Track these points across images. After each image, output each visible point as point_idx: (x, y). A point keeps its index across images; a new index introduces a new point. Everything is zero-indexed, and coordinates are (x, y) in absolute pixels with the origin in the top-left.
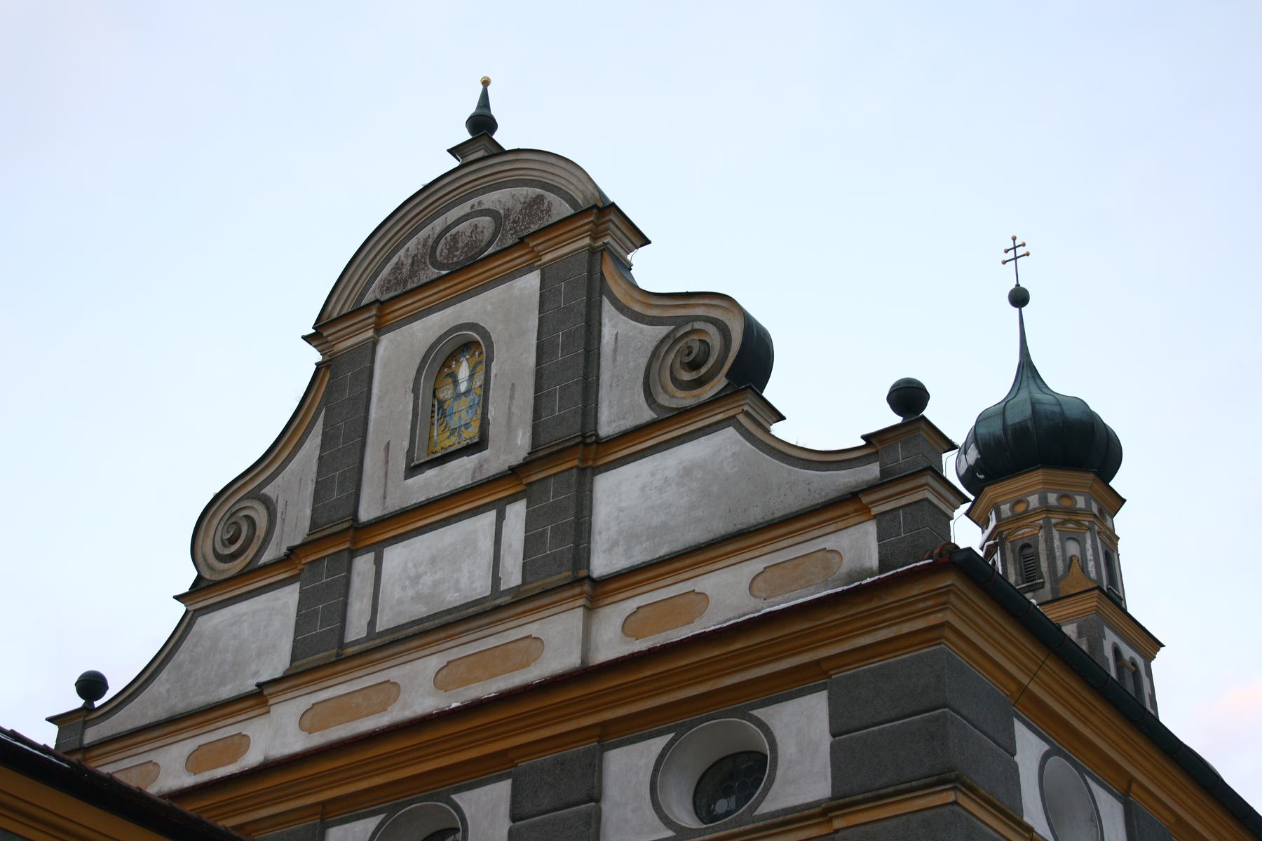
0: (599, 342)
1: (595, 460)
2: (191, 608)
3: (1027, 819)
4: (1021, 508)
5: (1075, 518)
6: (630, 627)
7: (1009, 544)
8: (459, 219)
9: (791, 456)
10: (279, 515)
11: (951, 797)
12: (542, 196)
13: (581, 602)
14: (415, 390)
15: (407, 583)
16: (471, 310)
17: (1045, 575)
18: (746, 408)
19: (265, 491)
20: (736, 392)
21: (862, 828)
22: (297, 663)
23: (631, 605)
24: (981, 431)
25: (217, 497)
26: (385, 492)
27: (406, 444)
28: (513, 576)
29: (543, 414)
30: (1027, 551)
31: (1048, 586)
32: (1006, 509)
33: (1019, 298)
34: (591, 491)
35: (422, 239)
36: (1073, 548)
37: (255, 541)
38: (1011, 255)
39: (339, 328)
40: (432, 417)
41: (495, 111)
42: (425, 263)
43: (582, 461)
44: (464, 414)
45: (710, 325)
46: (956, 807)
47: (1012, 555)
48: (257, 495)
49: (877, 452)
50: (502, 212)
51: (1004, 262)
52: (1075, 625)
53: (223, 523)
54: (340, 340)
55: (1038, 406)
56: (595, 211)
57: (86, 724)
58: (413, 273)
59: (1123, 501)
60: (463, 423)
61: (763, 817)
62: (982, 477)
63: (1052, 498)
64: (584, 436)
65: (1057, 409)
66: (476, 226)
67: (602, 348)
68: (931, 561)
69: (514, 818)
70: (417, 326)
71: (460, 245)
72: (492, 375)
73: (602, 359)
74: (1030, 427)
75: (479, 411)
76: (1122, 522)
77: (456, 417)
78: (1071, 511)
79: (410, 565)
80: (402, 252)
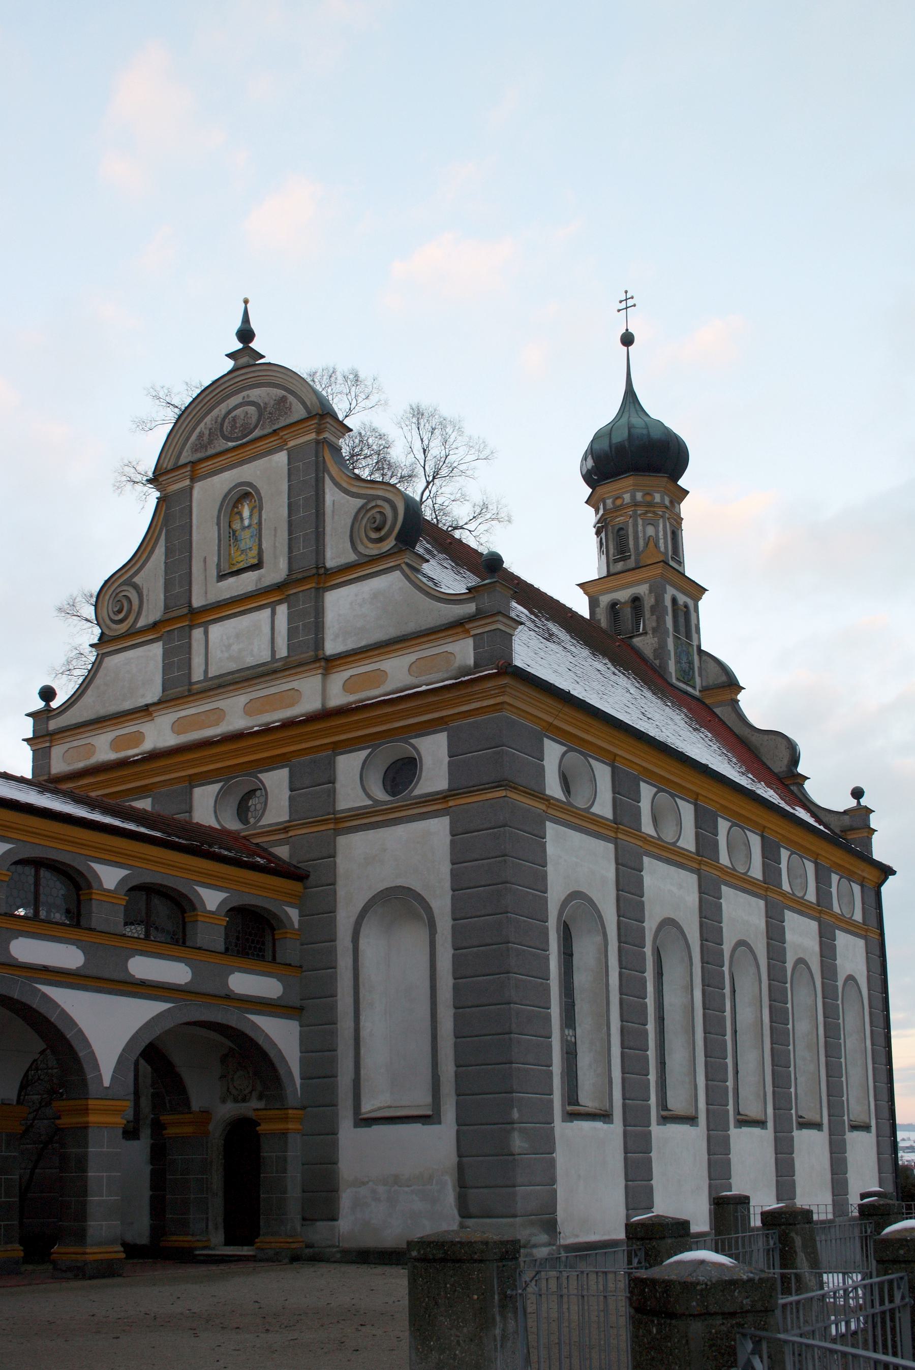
0: (324, 504)
1: (325, 583)
2: (100, 652)
3: (548, 792)
4: (619, 502)
5: (652, 509)
6: (348, 686)
7: (610, 527)
8: (236, 405)
9: (430, 594)
10: (145, 597)
11: (503, 793)
12: (286, 396)
13: (320, 671)
14: (218, 524)
15: (224, 649)
16: (249, 472)
17: (631, 550)
18: (407, 560)
19: (134, 580)
20: (400, 551)
21: (462, 807)
22: (166, 693)
23: (347, 674)
24: (596, 446)
25: (106, 582)
26: (206, 589)
27: (216, 559)
28: (282, 651)
29: (294, 551)
30: (622, 532)
31: (633, 557)
32: (609, 502)
33: (627, 340)
34: (323, 602)
35: (214, 418)
36: (650, 531)
37: (132, 611)
38: (623, 305)
39: (166, 477)
40: (230, 541)
41: (254, 325)
42: (217, 435)
43: (317, 583)
44: (248, 540)
45: (386, 503)
46: (506, 798)
47: (611, 535)
48: (129, 583)
49: (474, 597)
50: (262, 404)
51: (619, 311)
52: (648, 584)
53: (112, 599)
54: (170, 484)
55: (632, 430)
56: (318, 416)
57: (49, 719)
58: (210, 442)
59: (687, 492)
60: (248, 547)
61: (416, 797)
62: (596, 477)
63: (639, 496)
64: (317, 568)
65: (645, 432)
66: (247, 413)
67: (326, 509)
68: (496, 671)
69: (291, 790)
70: (216, 479)
71: (238, 425)
72: (263, 520)
73: (326, 516)
74: (627, 446)
75: (257, 540)
76: (686, 508)
77: (243, 542)
78: (650, 505)
79: (225, 637)
80: (202, 425)
